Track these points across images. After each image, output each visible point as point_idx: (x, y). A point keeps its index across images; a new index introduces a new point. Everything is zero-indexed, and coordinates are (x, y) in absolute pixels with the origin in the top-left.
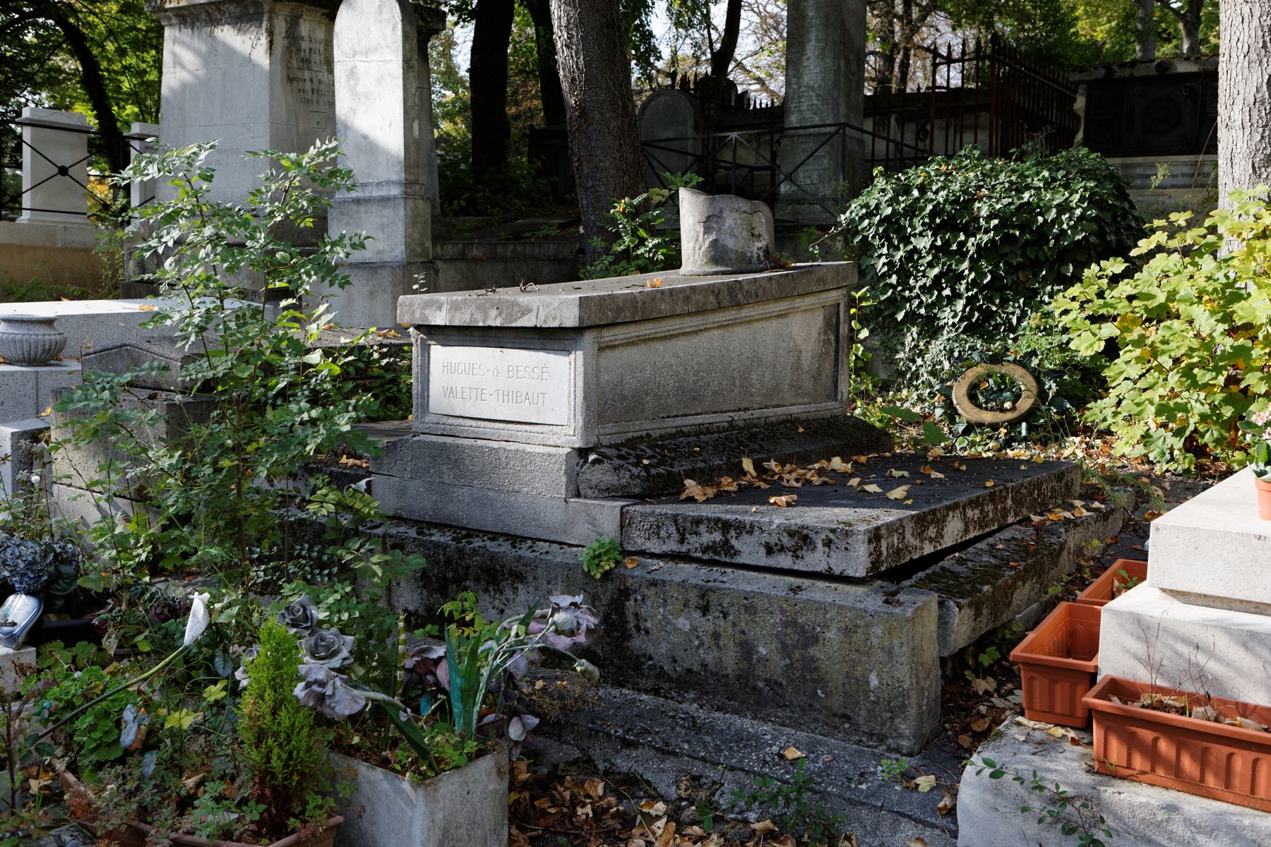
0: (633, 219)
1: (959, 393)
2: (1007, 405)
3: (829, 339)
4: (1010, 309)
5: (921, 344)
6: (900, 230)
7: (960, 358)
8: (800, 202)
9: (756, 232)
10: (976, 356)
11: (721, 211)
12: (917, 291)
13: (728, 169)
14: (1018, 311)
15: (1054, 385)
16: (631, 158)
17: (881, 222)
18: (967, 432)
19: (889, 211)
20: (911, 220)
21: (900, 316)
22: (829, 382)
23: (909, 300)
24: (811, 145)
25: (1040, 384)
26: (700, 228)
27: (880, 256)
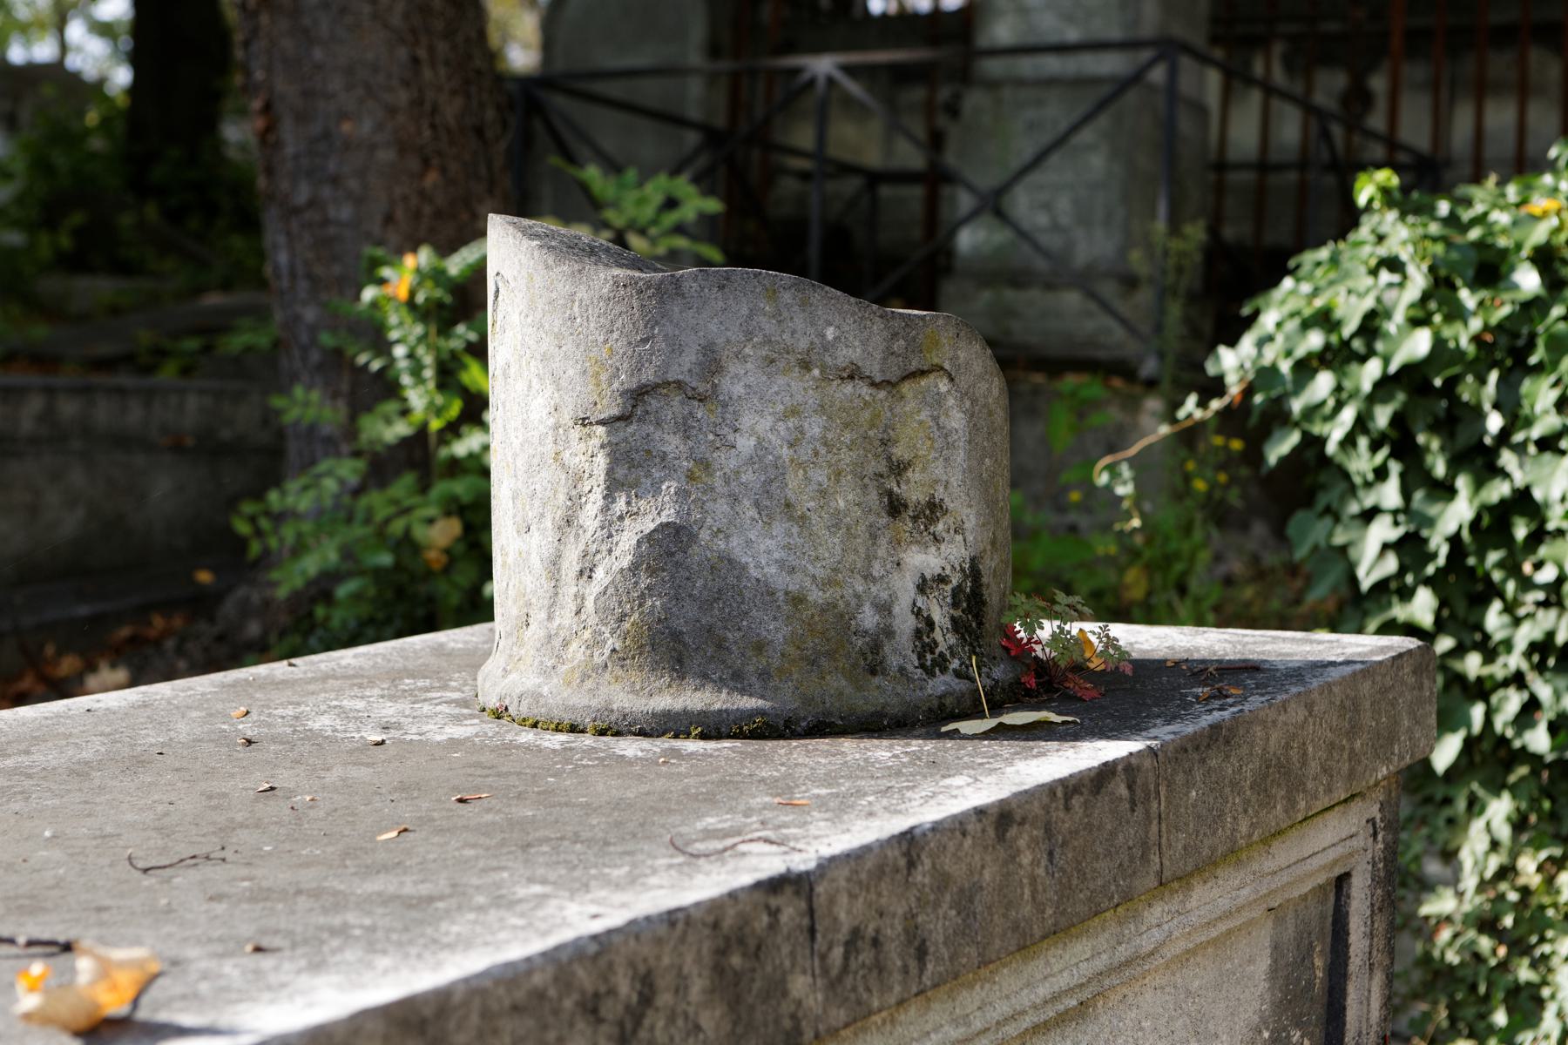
0: (445, 329)
5: (1528, 865)
6: (1456, 420)
8: (1018, 279)
9: (913, 491)
11: (712, 364)
12: (1516, 660)
13: (805, 176)
16: (451, 110)
17: (1385, 385)
19: (1419, 344)
20: (1509, 385)
21: (1446, 753)
23: (1482, 690)
24: (1056, 113)
26: (589, 456)
27: (1369, 515)
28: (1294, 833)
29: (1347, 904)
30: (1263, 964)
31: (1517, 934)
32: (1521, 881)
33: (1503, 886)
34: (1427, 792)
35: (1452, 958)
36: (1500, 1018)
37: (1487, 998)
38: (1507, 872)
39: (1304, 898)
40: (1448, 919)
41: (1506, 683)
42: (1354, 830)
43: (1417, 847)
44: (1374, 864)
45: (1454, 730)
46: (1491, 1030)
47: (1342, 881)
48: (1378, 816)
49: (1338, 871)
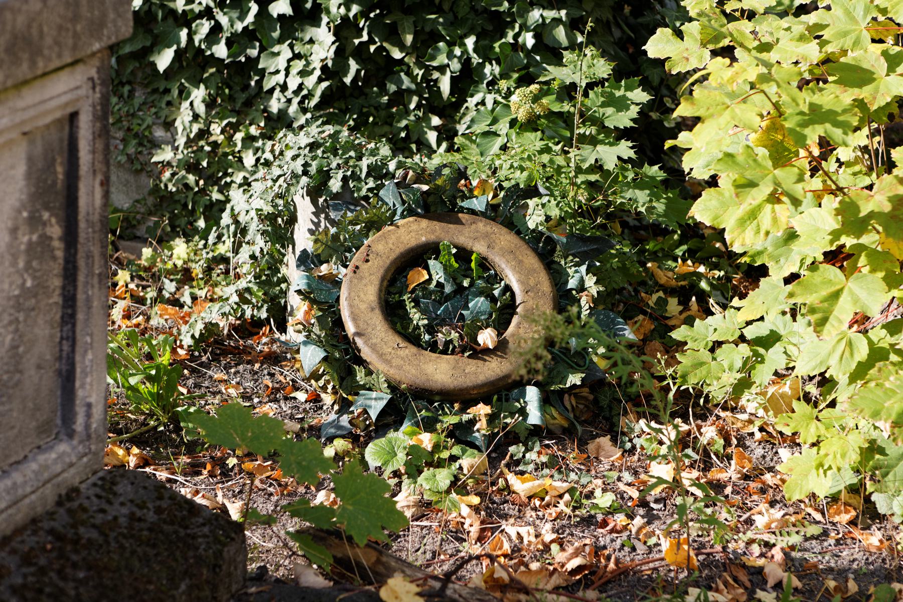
1: (358, 303)
2: (487, 337)
3: (45, 239)
4: (442, 59)
5: (216, 128)
7: (346, 198)
10: (389, 195)
14: (456, 66)
15: (590, 282)
18: (392, 417)
21: (164, 60)
22: (48, 381)
25: (557, 277)
28: (38, 83)
29: (77, 132)
30: (21, 169)
31: (211, 171)
32: (212, 139)
33: (202, 143)
34: (155, 86)
35: (172, 188)
36: (201, 223)
37: (194, 210)
38: (204, 133)
39: (47, 126)
40: (169, 164)
41: (200, 16)
42: (78, 83)
43: (149, 121)
44: (94, 106)
45: (169, 47)
46: (196, 231)
47: (73, 117)
48: (96, 76)
49: (70, 110)
